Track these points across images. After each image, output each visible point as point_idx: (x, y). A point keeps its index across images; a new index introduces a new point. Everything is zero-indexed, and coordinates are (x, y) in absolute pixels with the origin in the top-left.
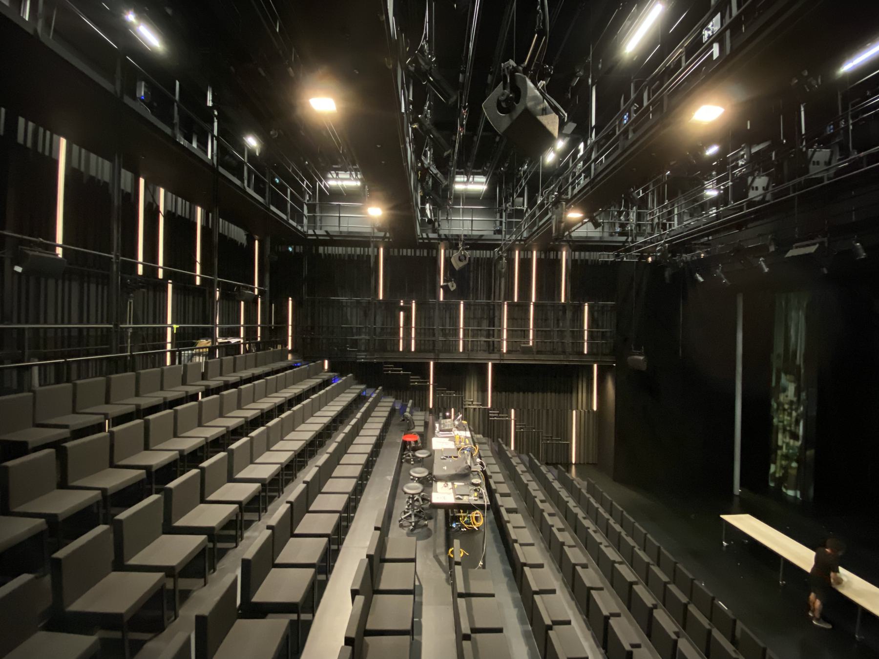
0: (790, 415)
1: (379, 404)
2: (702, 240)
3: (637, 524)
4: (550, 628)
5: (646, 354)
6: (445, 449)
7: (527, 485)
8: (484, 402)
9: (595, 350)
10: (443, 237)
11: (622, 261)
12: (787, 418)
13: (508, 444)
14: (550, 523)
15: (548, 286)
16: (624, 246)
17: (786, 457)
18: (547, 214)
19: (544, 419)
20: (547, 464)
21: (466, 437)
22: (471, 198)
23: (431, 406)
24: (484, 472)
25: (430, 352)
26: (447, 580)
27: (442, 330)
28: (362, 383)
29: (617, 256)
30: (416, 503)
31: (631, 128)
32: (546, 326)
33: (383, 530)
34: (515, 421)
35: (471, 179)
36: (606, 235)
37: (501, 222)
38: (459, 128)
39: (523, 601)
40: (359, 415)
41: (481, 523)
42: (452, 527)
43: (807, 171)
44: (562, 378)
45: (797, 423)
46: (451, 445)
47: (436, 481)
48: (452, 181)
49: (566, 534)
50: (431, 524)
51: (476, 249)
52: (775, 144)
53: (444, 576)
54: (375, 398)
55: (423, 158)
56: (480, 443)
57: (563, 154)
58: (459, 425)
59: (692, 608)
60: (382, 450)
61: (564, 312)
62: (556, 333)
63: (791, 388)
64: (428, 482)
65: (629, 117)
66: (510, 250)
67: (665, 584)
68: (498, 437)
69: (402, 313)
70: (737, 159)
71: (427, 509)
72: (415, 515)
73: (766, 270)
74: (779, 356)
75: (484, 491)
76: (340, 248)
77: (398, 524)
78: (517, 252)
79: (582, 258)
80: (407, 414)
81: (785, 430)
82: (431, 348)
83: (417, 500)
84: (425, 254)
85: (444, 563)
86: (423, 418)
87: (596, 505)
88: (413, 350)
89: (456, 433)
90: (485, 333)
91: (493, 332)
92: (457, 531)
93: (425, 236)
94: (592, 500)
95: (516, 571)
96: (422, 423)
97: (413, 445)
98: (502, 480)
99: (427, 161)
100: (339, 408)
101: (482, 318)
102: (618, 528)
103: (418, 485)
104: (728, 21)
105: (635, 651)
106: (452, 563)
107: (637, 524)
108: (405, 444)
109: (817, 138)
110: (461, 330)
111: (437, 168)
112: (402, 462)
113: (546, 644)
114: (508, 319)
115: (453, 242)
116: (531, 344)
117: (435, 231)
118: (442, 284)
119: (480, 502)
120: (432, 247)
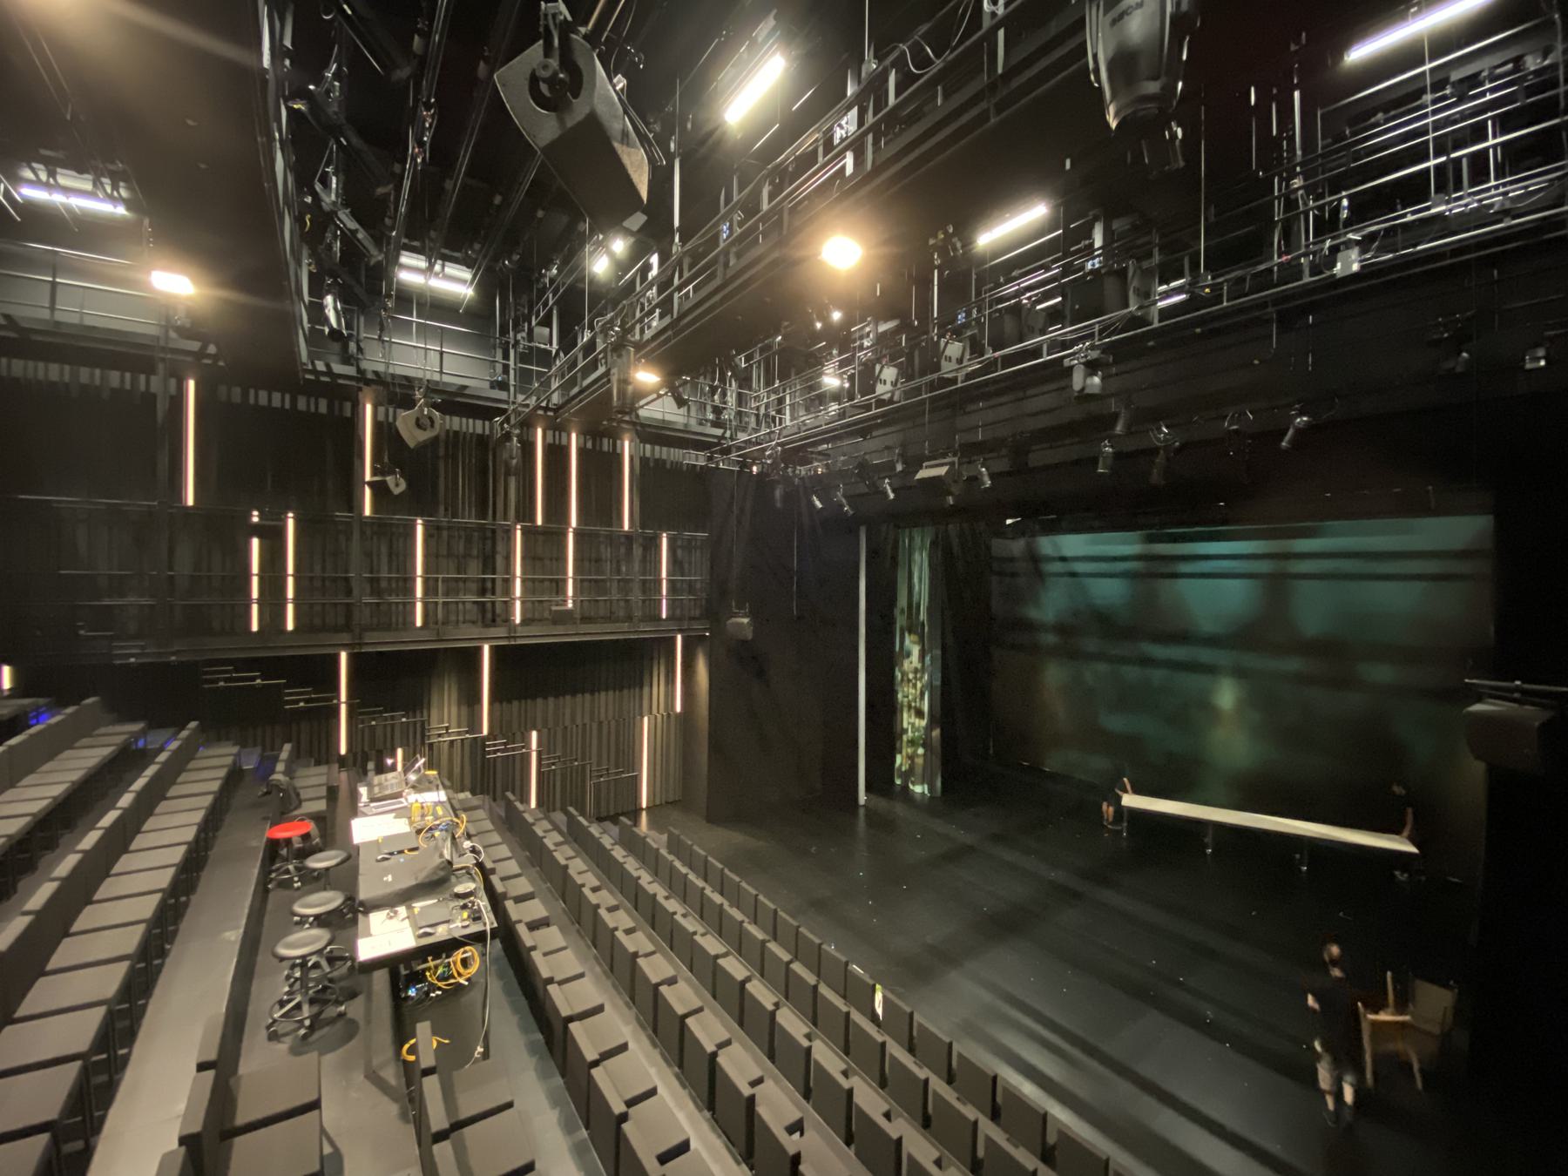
0: (915, 686)
1: (172, 792)
2: (820, 448)
3: (744, 884)
4: (624, 1117)
5: (752, 614)
6: (386, 839)
7: (566, 867)
8: (474, 724)
9: (678, 612)
10: (370, 376)
11: (717, 468)
12: (912, 691)
13: (525, 799)
14: (611, 925)
15: (600, 502)
16: (719, 444)
17: (912, 742)
18: (596, 368)
19: (595, 742)
20: (600, 819)
21: (440, 803)
22: (439, 308)
23: (343, 751)
24: (480, 865)
25: (336, 629)
26: (404, 1116)
27: (371, 580)
28: (133, 720)
29: (710, 459)
30: (314, 974)
31: (734, 249)
32: (598, 572)
33: (222, 1067)
34: (539, 754)
35: (437, 268)
36: (693, 422)
37: (506, 369)
38: (412, 148)
39: (568, 1089)
40: (126, 800)
41: (473, 969)
42: (408, 998)
43: (937, 368)
44: (624, 663)
45: (922, 694)
46: (401, 826)
47: (366, 913)
48: (394, 261)
49: (639, 935)
50: (354, 1009)
51: (452, 413)
52: (905, 326)
53: (394, 1109)
54: (175, 753)
55: (318, 187)
56: (465, 810)
57: (622, 267)
58: (419, 781)
59: (824, 990)
60: (205, 875)
61: (630, 550)
62: (615, 584)
63: (916, 651)
64: (345, 919)
65: (730, 228)
66: (527, 424)
67: (763, 942)
68: (506, 789)
69: (255, 542)
70: (861, 338)
71: (341, 978)
72: (312, 1002)
73: (892, 496)
74: (902, 611)
75: (483, 903)
77: (264, 1033)
78: (539, 432)
79: (657, 456)
80: (279, 777)
81: (910, 707)
82: (341, 621)
83: (316, 966)
84: (323, 408)
85: (393, 1081)
86: (323, 780)
87: (684, 870)
88: (290, 626)
89: (412, 798)
90: (474, 586)
91: (492, 585)
92: (420, 1001)
93: (320, 366)
94: (678, 864)
95: (552, 1034)
96: (323, 791)
97: (297, 844)
98: (517, 870)
99: (330, 197)
100: (57, 790)
101: (467, 555)
102: (717, 898)
103: (315, 932)
104: (870, 119)
105: (757, 1090)
106: (412, 1074)
107: (744, 884)
108: (273, 850)
109: (949, 327)
110: (419, 582)
111: (355, 215)
112: (267, 891)
113: (618, 1147)
114: (523, 558)
115: (398, 392)
116: (570, 605)
117: (347, 359)
118: (368, 478)
119: (476, 928)
120: (343, 395)
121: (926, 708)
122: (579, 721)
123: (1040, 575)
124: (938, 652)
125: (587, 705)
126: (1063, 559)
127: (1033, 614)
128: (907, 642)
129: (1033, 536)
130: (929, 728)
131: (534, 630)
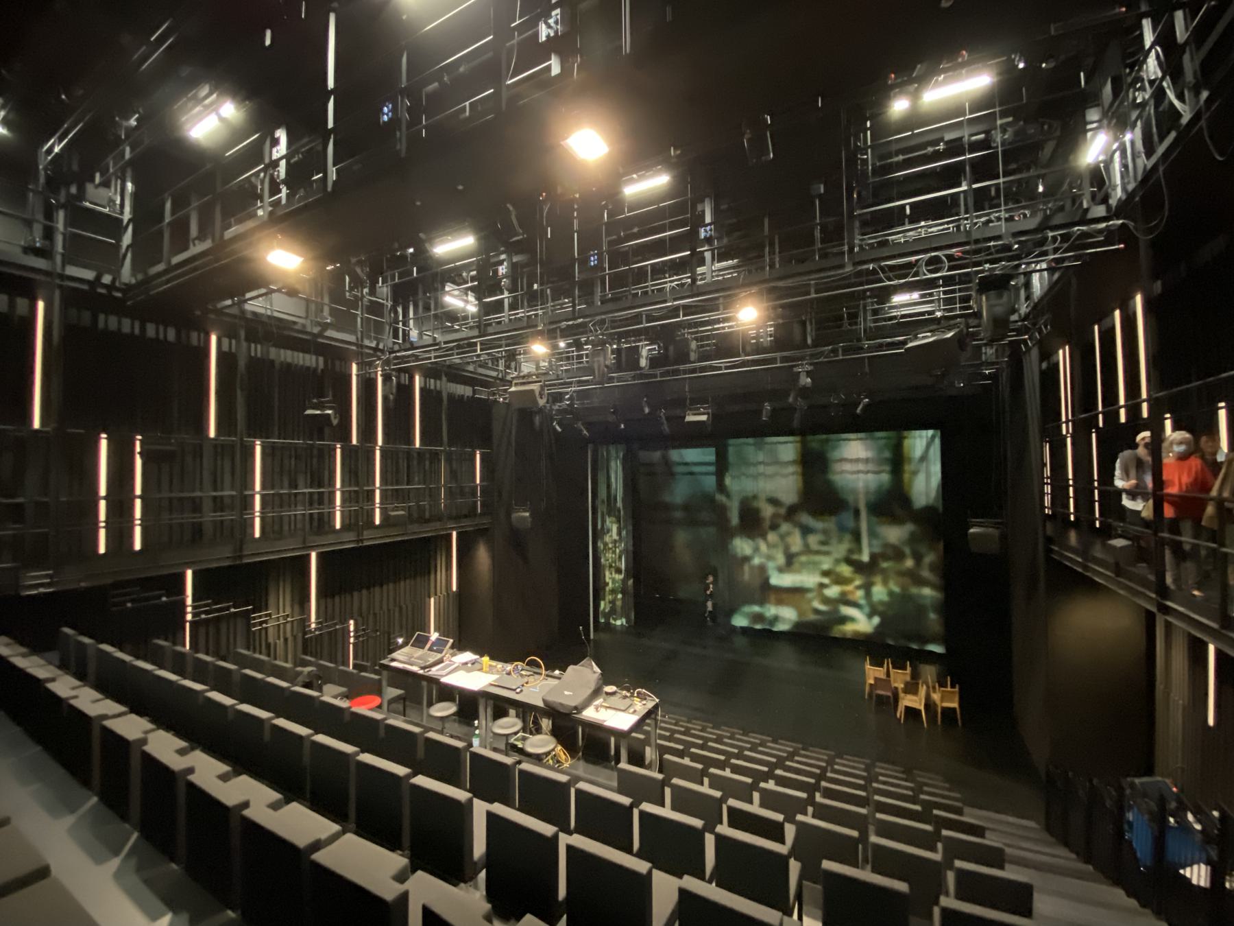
0: (614, 552)
17: (613, 591)
45: (620, 558)
76: (307, 356)
121: (623, 567)
122: (385, 607)
123: (672, 474)
124: (630, 528)
125: (391, 594)
126: (686, 464)
127: (667, 498)
128: (608, 520)
129: (667, 448)
130: (624, 581)
131: (351, 536)
